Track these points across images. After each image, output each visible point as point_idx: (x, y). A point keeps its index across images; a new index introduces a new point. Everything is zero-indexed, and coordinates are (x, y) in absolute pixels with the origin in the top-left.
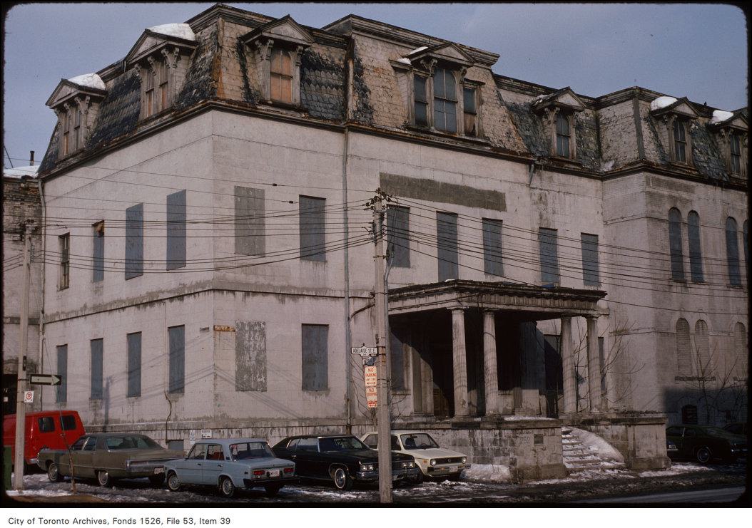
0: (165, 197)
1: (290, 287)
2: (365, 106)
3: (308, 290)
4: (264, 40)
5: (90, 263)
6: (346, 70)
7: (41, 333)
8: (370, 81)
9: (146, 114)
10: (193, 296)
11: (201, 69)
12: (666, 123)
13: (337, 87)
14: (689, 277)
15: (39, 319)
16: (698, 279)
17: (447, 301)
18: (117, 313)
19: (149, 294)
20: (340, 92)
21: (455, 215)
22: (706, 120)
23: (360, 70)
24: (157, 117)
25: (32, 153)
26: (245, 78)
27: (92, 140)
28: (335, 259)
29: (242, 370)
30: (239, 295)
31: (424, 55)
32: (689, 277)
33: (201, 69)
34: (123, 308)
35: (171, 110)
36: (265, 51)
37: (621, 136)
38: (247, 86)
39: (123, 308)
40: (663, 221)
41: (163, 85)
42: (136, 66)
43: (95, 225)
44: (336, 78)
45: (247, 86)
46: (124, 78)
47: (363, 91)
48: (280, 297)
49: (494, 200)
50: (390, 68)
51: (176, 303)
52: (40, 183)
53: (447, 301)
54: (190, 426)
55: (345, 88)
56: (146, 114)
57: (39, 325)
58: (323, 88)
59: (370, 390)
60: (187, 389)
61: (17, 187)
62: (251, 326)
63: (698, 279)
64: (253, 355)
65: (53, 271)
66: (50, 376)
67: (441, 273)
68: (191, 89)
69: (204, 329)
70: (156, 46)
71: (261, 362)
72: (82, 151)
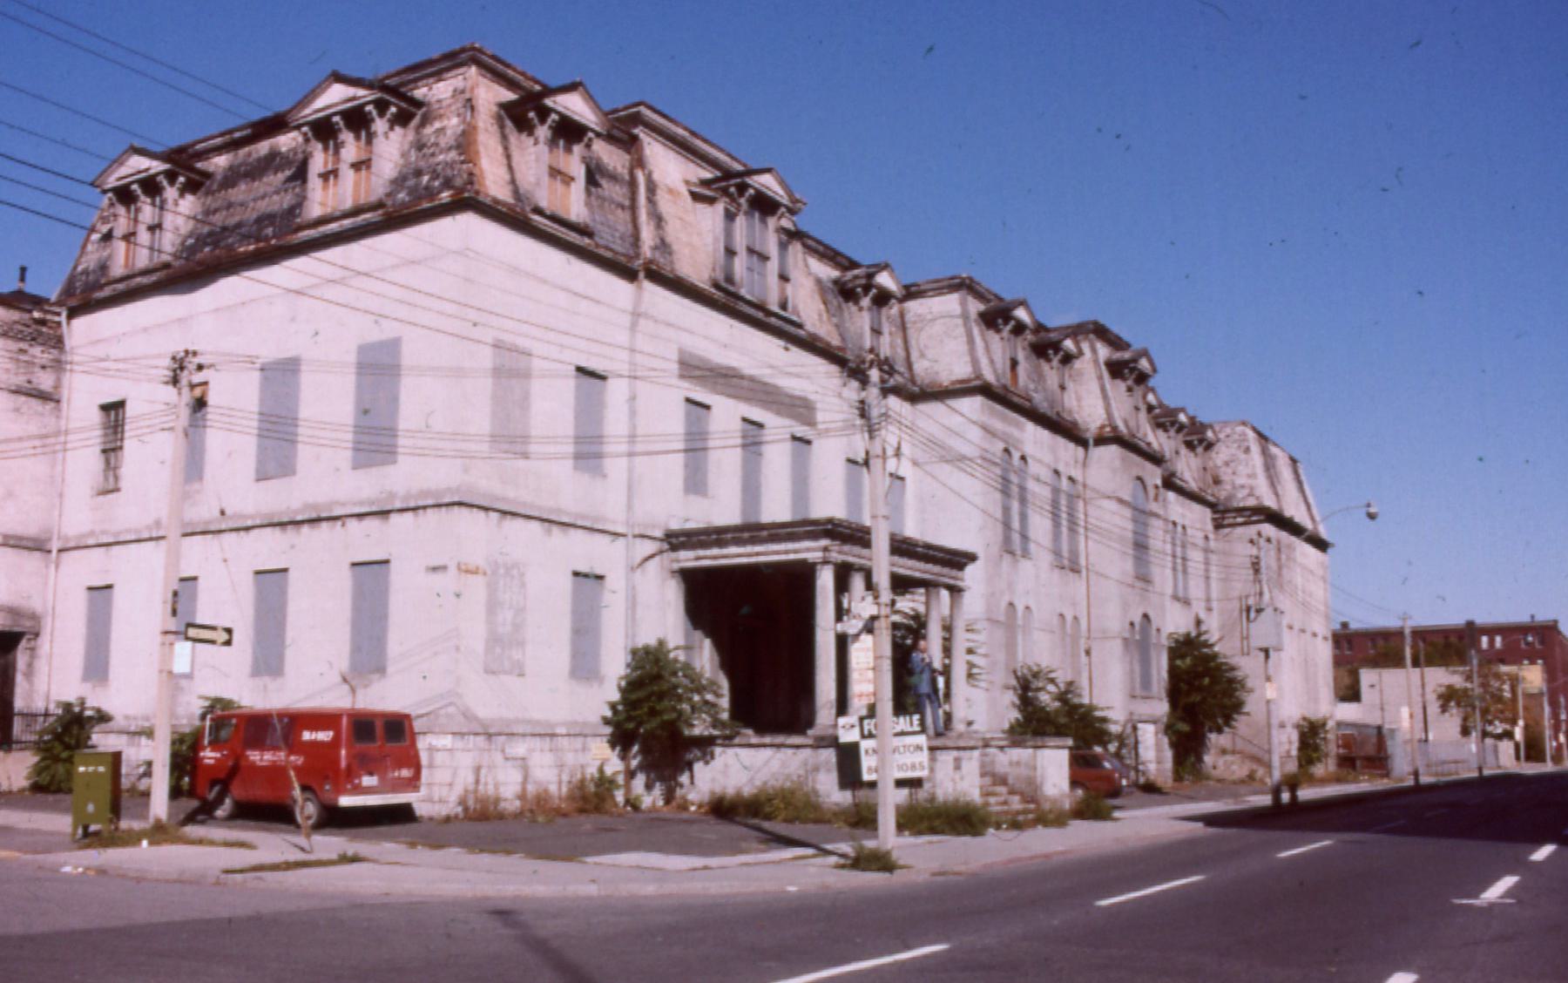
0: (353, 348)
1: (559, 511)
2: (663, 241)
3: (583, 517)
4: (544, 113)
5: (908, 325)
6: (633, 184)
7: (53, 567)
8: (665, 204)
9: (314, 210)
10: (339, 523)
11: (436, 144)
12: (998, 331)
13: (623, 207)
14: (1019, 552)
15: (50, 539)
16: (1026, 554)
17: (808, 550)
18: (305, 529)
19: (307, 507)
20: (626, 216)
21: (760, 426)
22: (1028, 332)
23: (652, 188)
24: (346, 215)
25: (23, 270)
26: (510, 168)
27: (187, 250)
28: (616, 468)
29: (494, 640)
30: (494, 515)
31: (738, 180)
32: (1019, 552)
33: (436, 144)
34: (247, 529)
35: (380, 205)
36: (543, 132)
37: (942, 341)
38: (513, 181)
39: (247, 529)
40: (995, 464)
41: (357, 166)
42: (305, 129)
43: (106, 408)
44: (620, 192)
45: (513, 181)
46: (249, 154)
47: (658, 220)
48: (546, 524)
49: (800, 409)
50: (686, 194)
51: (372, 524)
52: (64, 314)
53: (808, 550)
54: (559, 730)
55: (633, 208)
56: (314, 210)
57: (50, 552)
58: (606, 204)
59: (861, 674)
60: (390, 669)
61: (26, 316)
62: (508, 569)
63: (1026, 554)
64: (509, 615)
65: (85, 460)
66: (213, 628)
67: (744, 512)
68: (418, 173)
69: (435, 569)
70: (354, 99)
71: (517, 627)
72: (166, 266)
